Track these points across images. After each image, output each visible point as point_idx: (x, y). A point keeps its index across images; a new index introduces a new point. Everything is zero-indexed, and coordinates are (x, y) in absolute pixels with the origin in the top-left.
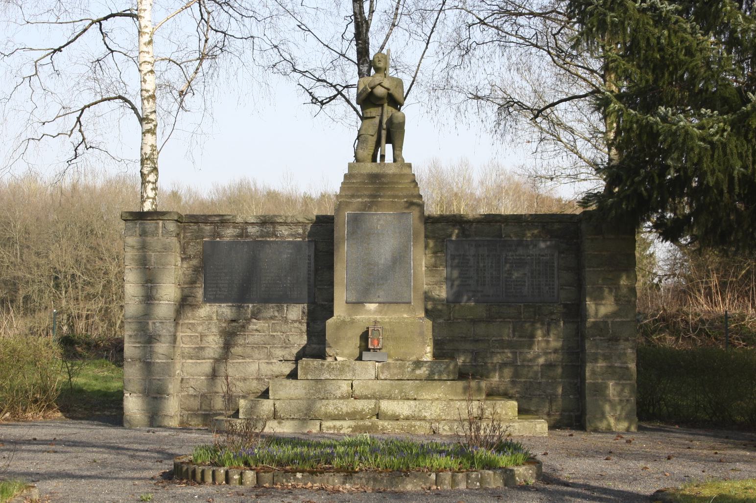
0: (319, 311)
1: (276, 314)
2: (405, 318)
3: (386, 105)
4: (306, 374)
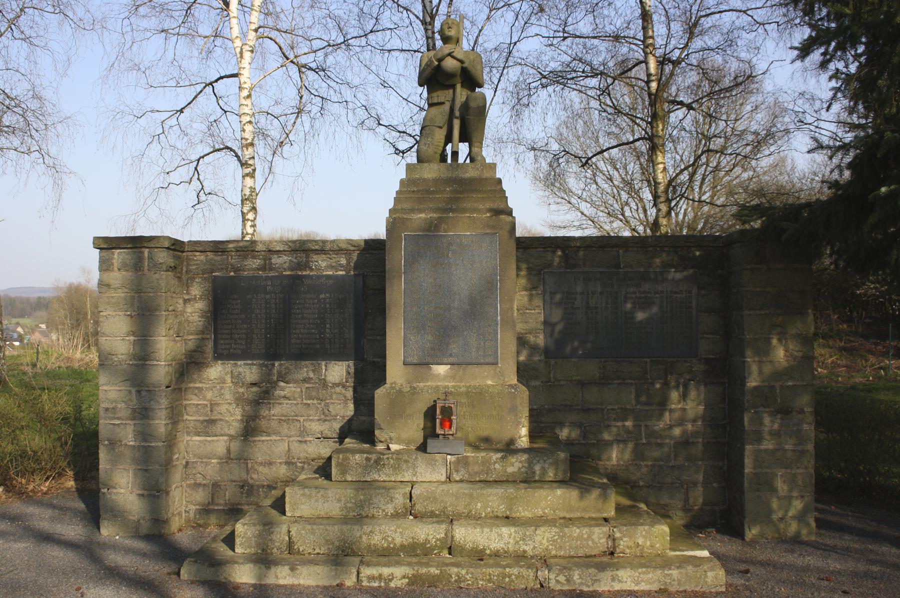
0: (369, 374)
1: (311, 375)
2: (489, 386)
3: (459, 86)
4: (344, 473)
